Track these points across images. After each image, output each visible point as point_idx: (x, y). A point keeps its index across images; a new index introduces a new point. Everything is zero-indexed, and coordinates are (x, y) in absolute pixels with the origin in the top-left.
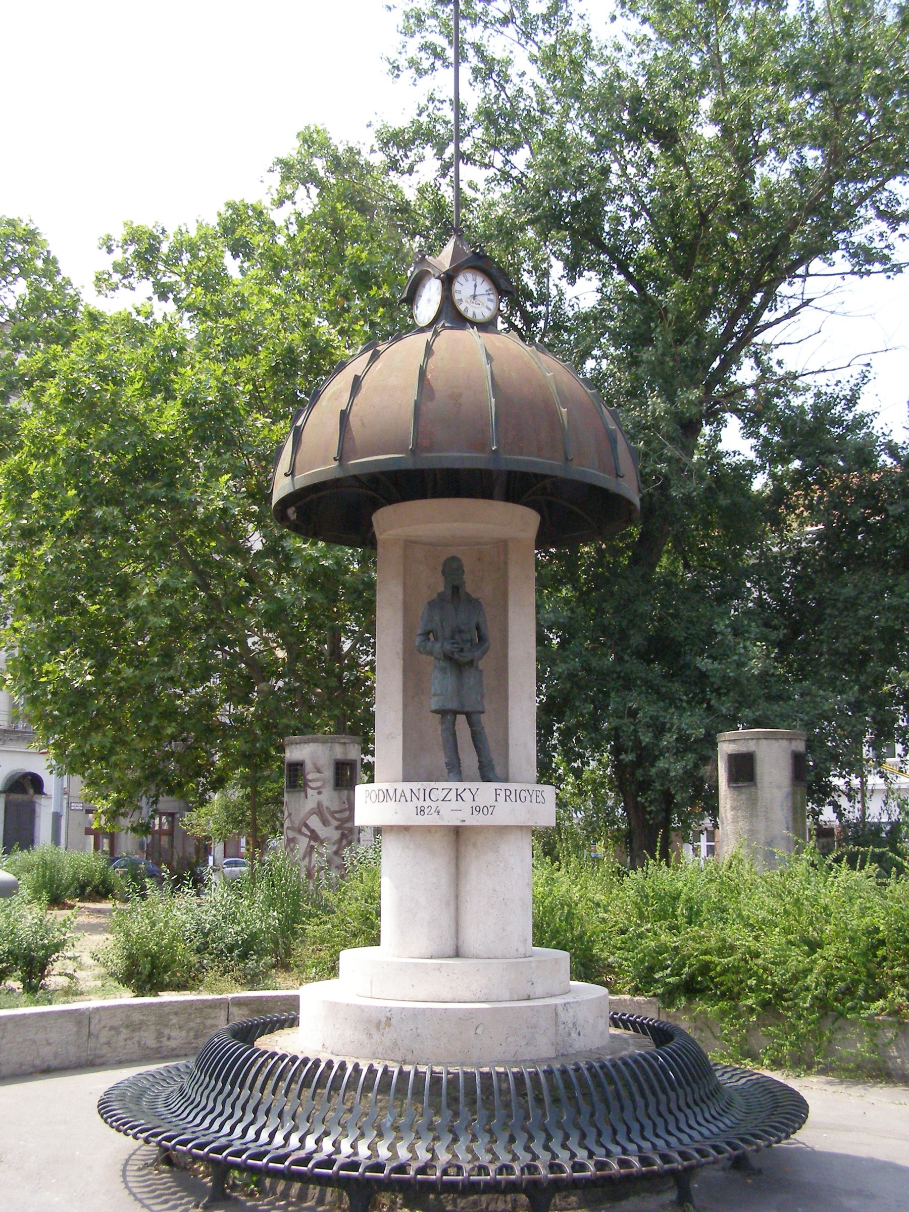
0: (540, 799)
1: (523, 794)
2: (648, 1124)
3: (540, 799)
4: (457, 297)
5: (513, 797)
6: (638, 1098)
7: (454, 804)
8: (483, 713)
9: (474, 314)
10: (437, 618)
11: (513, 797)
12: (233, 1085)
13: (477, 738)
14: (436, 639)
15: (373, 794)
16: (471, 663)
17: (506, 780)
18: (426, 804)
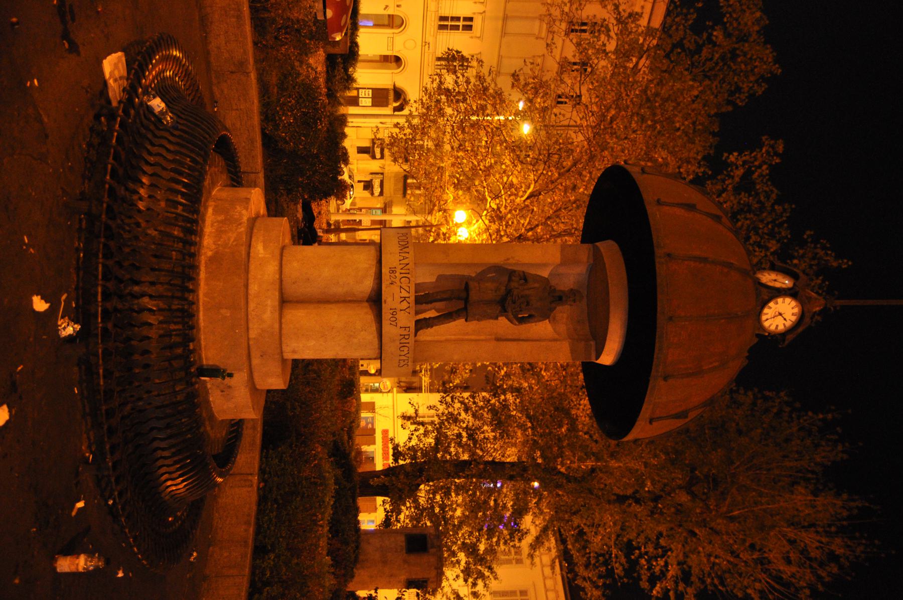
1: (406, 349)
3: (402, 363)
4: (780, 300)
5: (404, 341)
8: (466, 320)
9: (770, 308)
10: (536, 285)
11: (404, 341)
12: (179, 137)
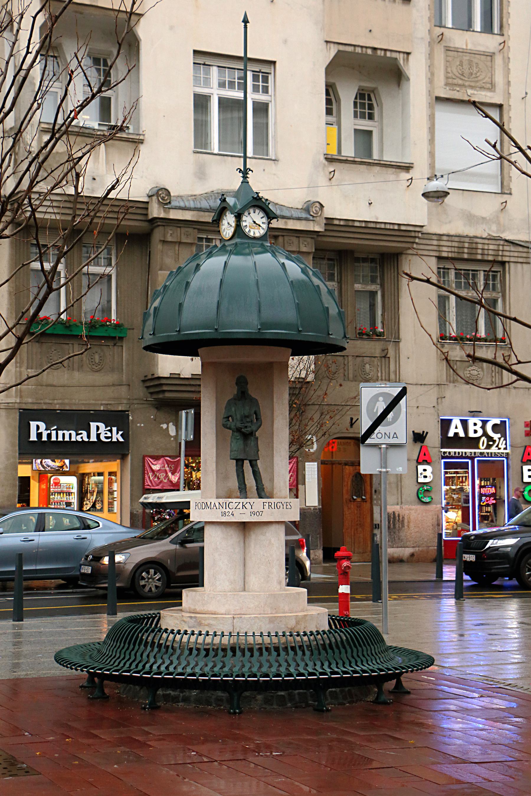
0: (289, 507)
2: (353, 661)
6: (347, 647)
7: (241, 511)
13: (256, 474)
14: (233, 420)
15: (199, 505)
16: (252, 434)
17: (271, 497)
18: (227, 511)
